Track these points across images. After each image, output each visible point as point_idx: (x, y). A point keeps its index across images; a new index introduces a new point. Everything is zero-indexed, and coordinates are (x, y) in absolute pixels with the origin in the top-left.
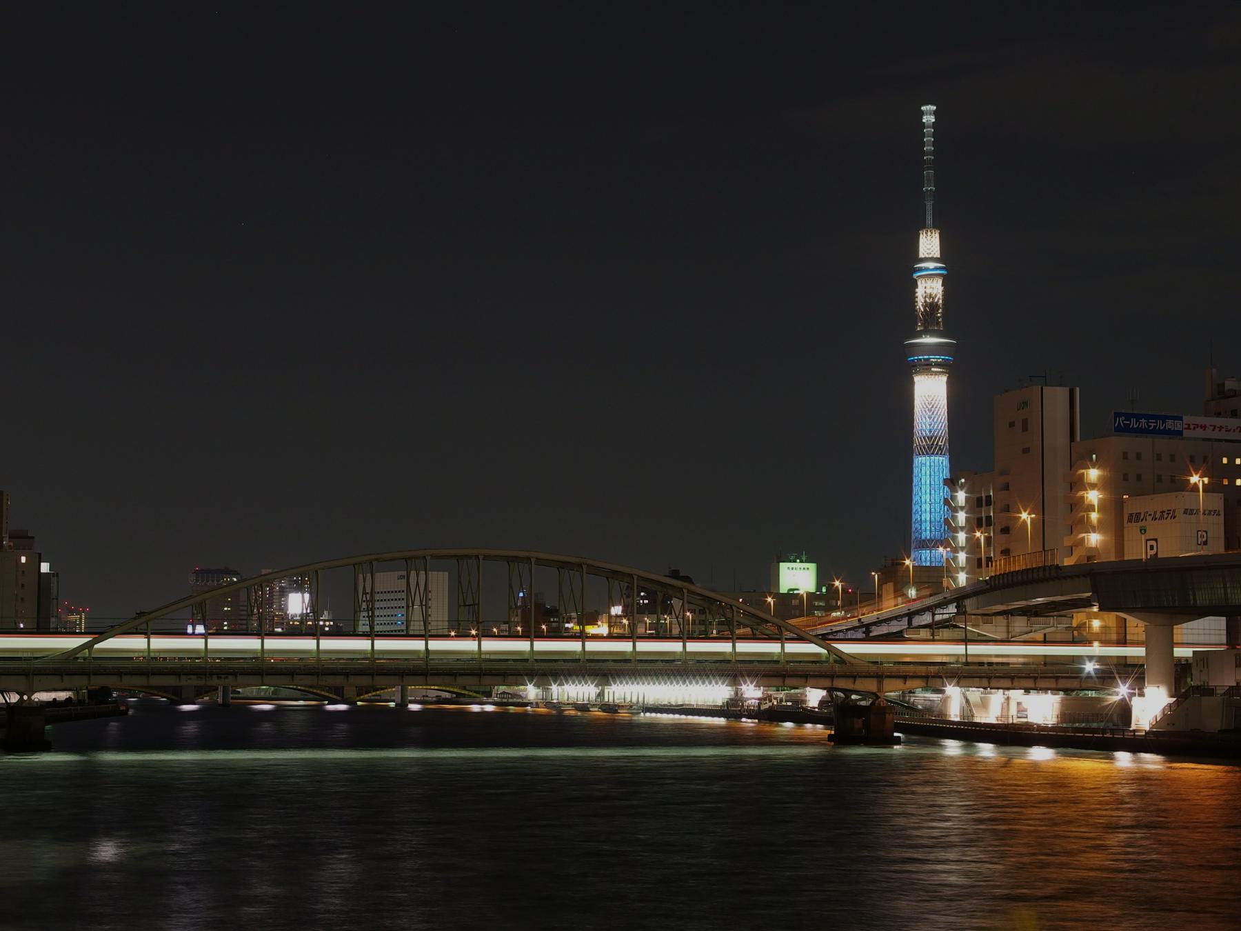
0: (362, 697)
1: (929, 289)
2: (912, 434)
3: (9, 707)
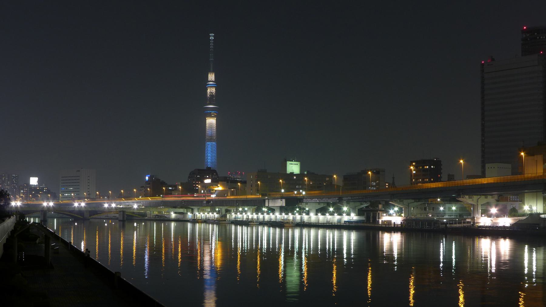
0: (92, 217)
1: (211, 90)
2: (205, 135)
3: (523, 304)
